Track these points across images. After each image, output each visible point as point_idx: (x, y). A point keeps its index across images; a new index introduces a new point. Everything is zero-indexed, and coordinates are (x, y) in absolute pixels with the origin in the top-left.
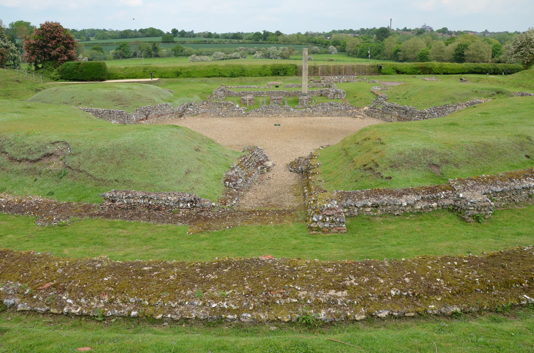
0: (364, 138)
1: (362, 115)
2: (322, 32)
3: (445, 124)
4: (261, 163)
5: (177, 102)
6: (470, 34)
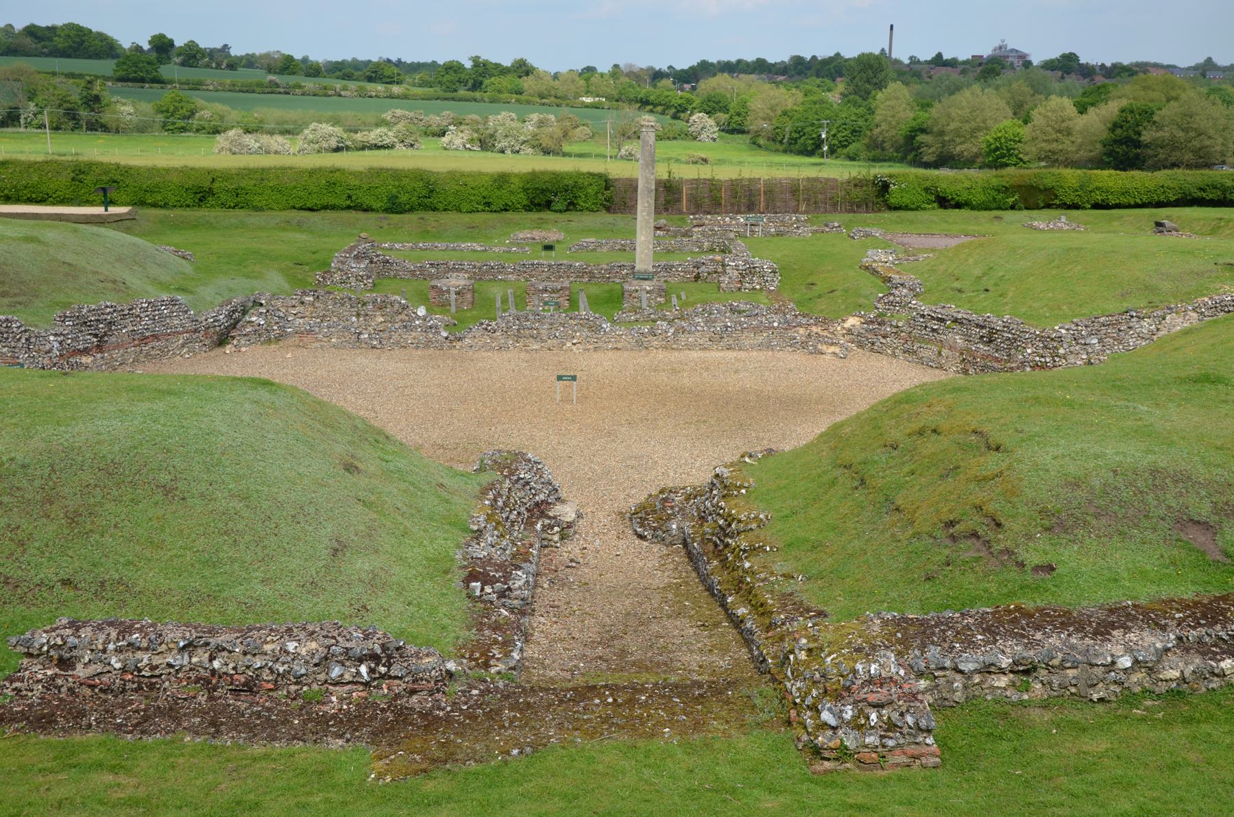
0: (915, 426)
1: (842, 346)
2: (665, 68)
3: (1182, 381)
4: (540, 509)
5: (207, 292)
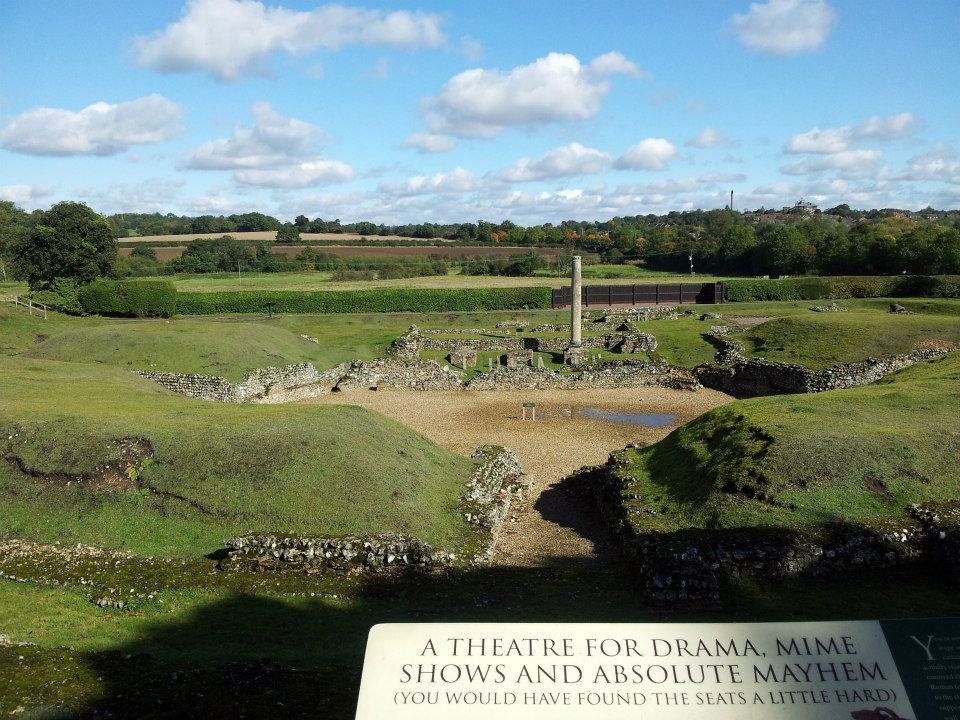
6: (898, 217)
